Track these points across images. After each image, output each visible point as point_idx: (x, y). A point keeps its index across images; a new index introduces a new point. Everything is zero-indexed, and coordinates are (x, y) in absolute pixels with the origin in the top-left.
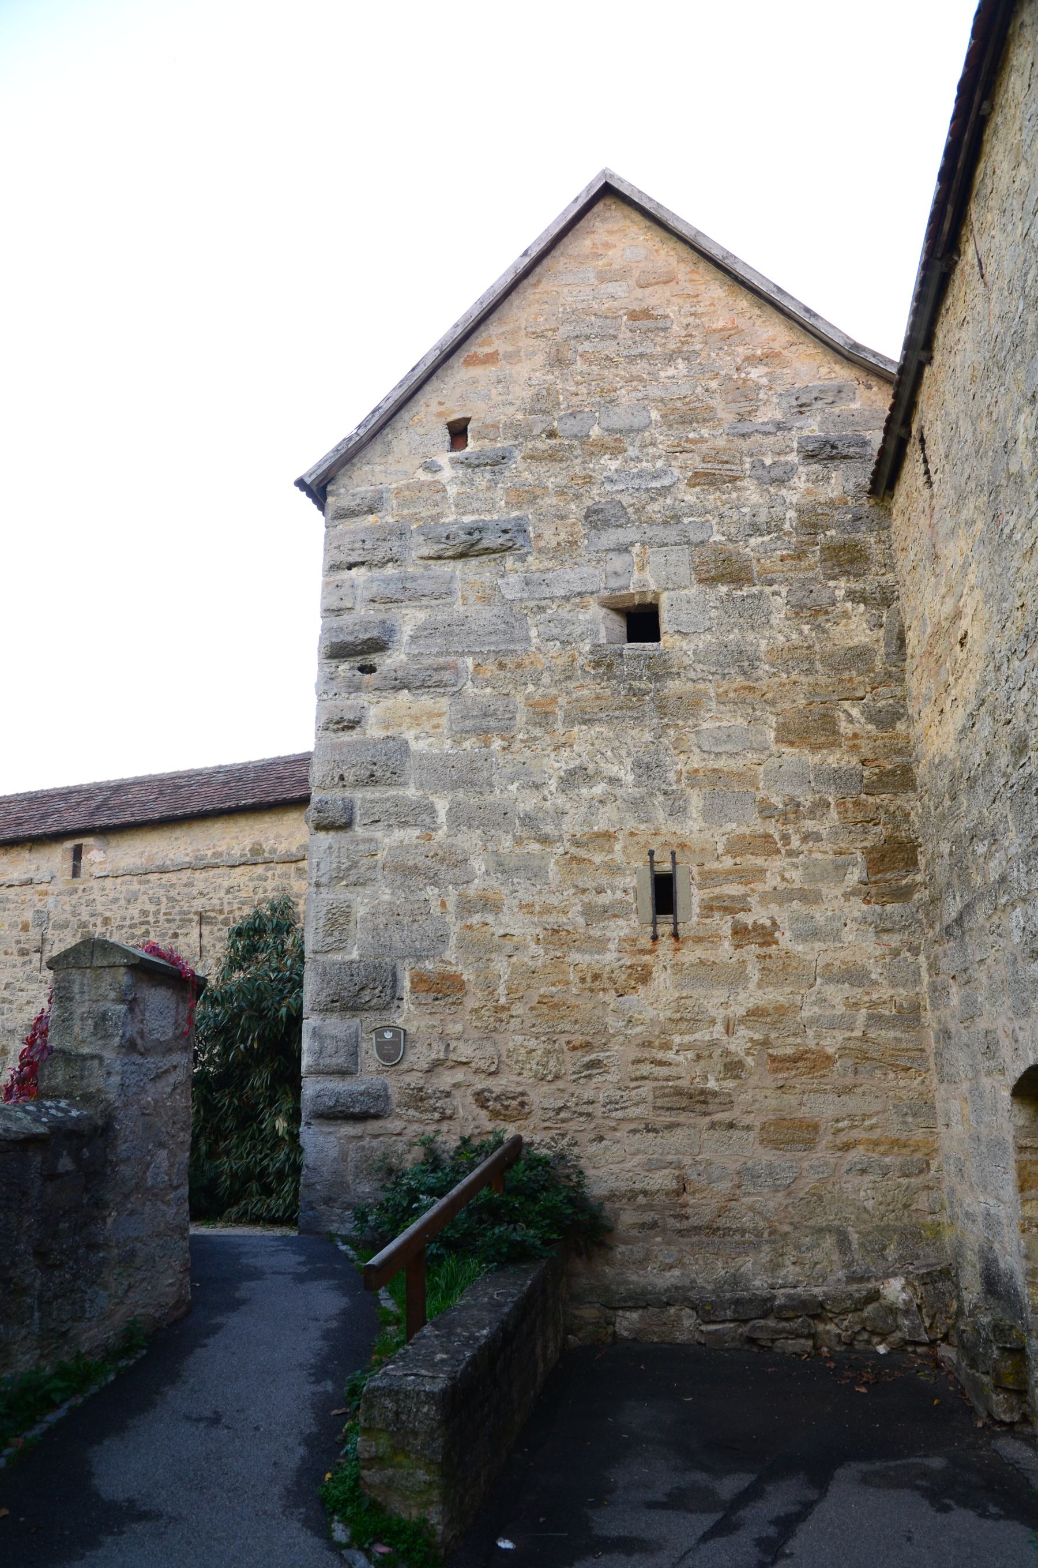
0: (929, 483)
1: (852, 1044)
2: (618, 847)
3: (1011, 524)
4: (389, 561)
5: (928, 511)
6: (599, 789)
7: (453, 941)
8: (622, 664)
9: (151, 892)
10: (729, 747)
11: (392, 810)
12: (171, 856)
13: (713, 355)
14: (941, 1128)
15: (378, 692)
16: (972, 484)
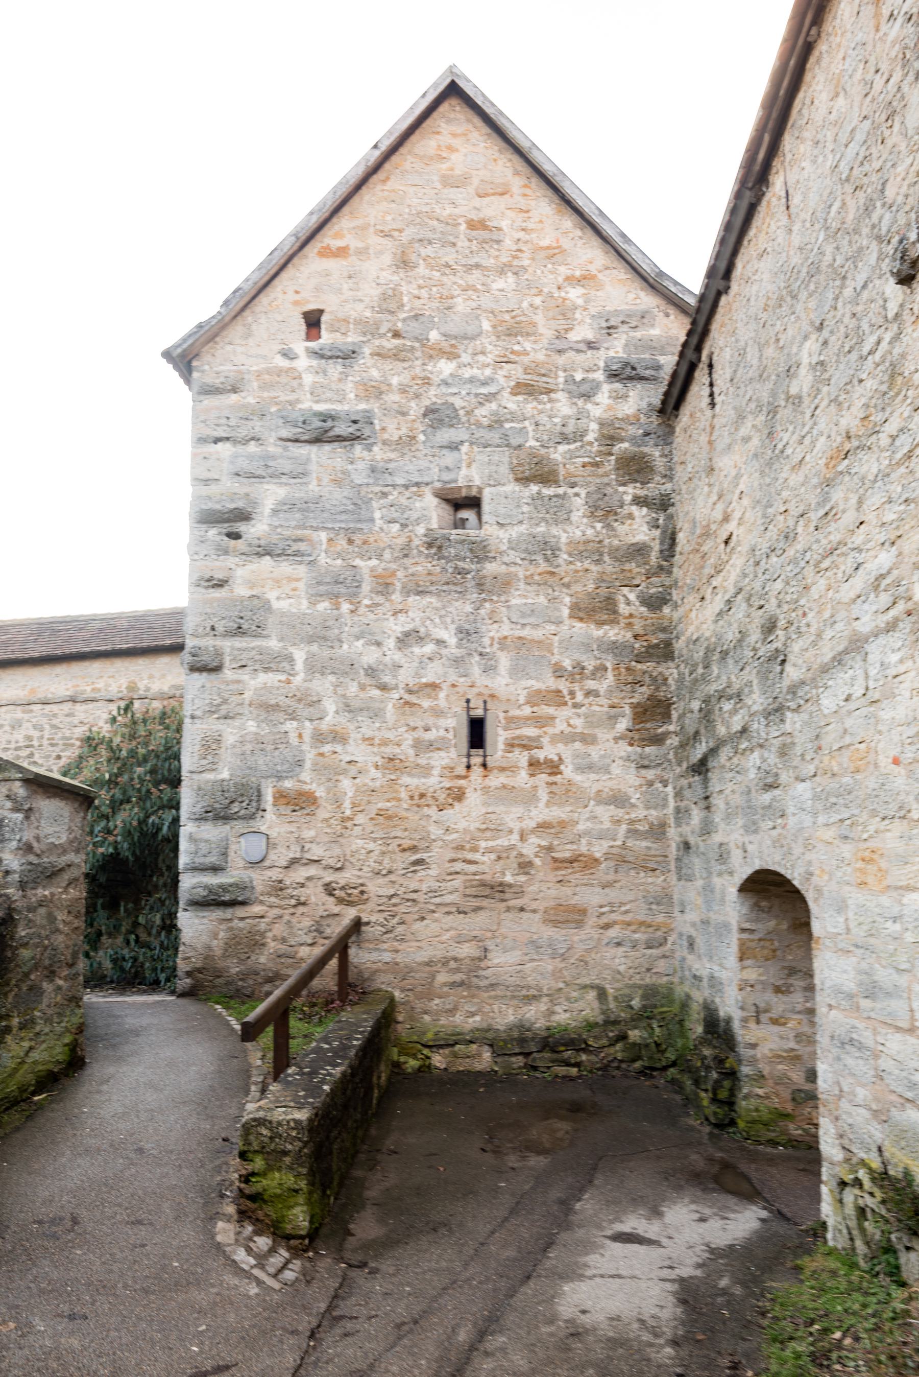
0: (713, 404)
1: (614, 851)
2: (442, 695)
3: (785, 441)
4: (253, 439)
5: (708, 429)
6: (429, 648)
7: (308, 765)
8: (450, 546)
9: (34, 720)
10: (532, 620)
11: (258, 657)
12: (52, 690)
13: (539, 272)
14: (676, 913)
15: (244, 557)
16: (753, 405)
